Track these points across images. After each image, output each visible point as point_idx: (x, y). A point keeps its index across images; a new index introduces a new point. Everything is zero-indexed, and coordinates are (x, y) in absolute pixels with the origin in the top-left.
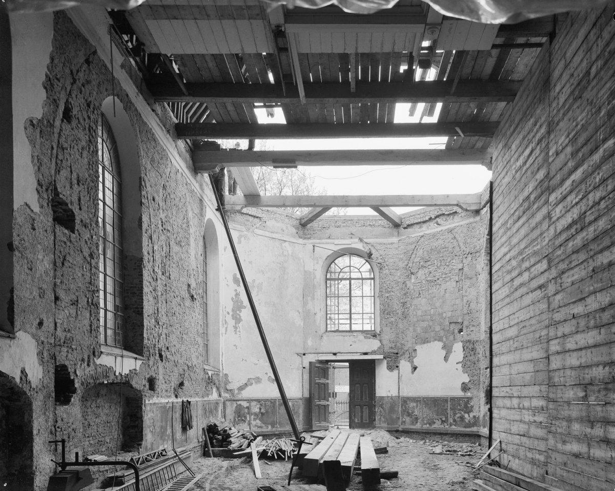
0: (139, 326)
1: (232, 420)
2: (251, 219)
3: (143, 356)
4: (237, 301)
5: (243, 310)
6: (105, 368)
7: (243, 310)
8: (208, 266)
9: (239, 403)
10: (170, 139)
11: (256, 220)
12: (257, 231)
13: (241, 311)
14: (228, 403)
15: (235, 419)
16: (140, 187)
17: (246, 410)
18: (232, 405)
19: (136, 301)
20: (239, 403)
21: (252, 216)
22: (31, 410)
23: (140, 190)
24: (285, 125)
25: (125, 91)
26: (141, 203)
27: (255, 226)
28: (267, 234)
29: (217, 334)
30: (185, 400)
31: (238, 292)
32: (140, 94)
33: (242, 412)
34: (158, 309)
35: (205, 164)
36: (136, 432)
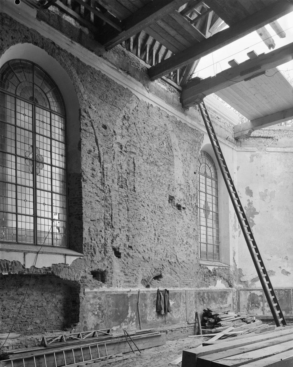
1: (246, 306)
2: (263, 140)
3: (83, 253)
4: (250, 209)
5: (255, 216)
7: (255, 216)
8: (218, 183)
9: (252, 292)
11: (269, 140)
12: (269, 149)
13: (253, 217)
14: (242, 293)
15: (248, 306)
16: (80, 117)
17: (260, 298)
18: (245, 294)
20: (252, 292)
21: (264, 137)
23: (80, 119)
24: (229, 28)
26: (81, 129)
27: (267, 145)
28: (279, 149)
29: (227, 237)
30: (161, 289)
31: (251, 201)
33: (256, 300)
35: (190, 98)
36: (75, 315)
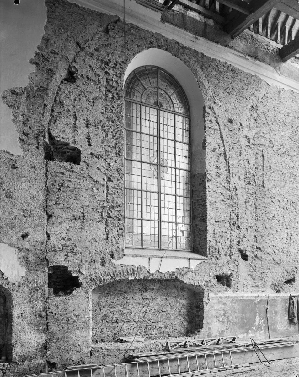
0: (203, 231)
6: (132, 267)
10: (271, 68)
19: (201, 211)
22: (11, 299)
25: (173, 40)
32: (198, 37)
34: (237, 216)
